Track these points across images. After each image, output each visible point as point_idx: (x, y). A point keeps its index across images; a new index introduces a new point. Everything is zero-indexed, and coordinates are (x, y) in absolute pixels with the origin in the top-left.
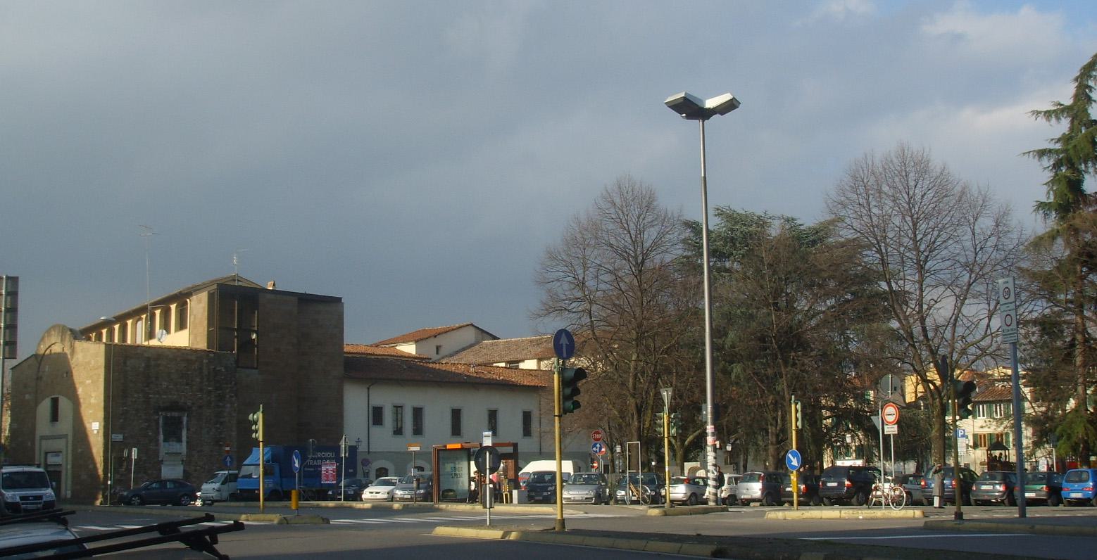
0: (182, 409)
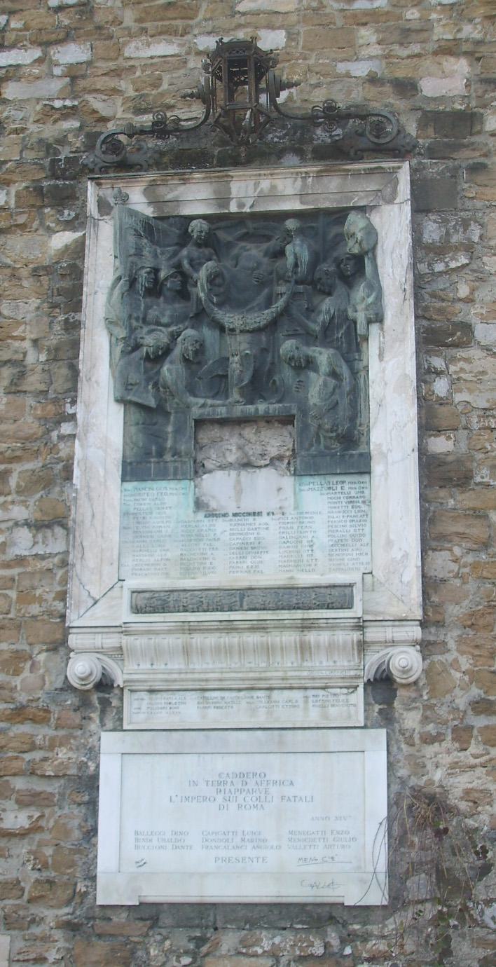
0: (350, 138)
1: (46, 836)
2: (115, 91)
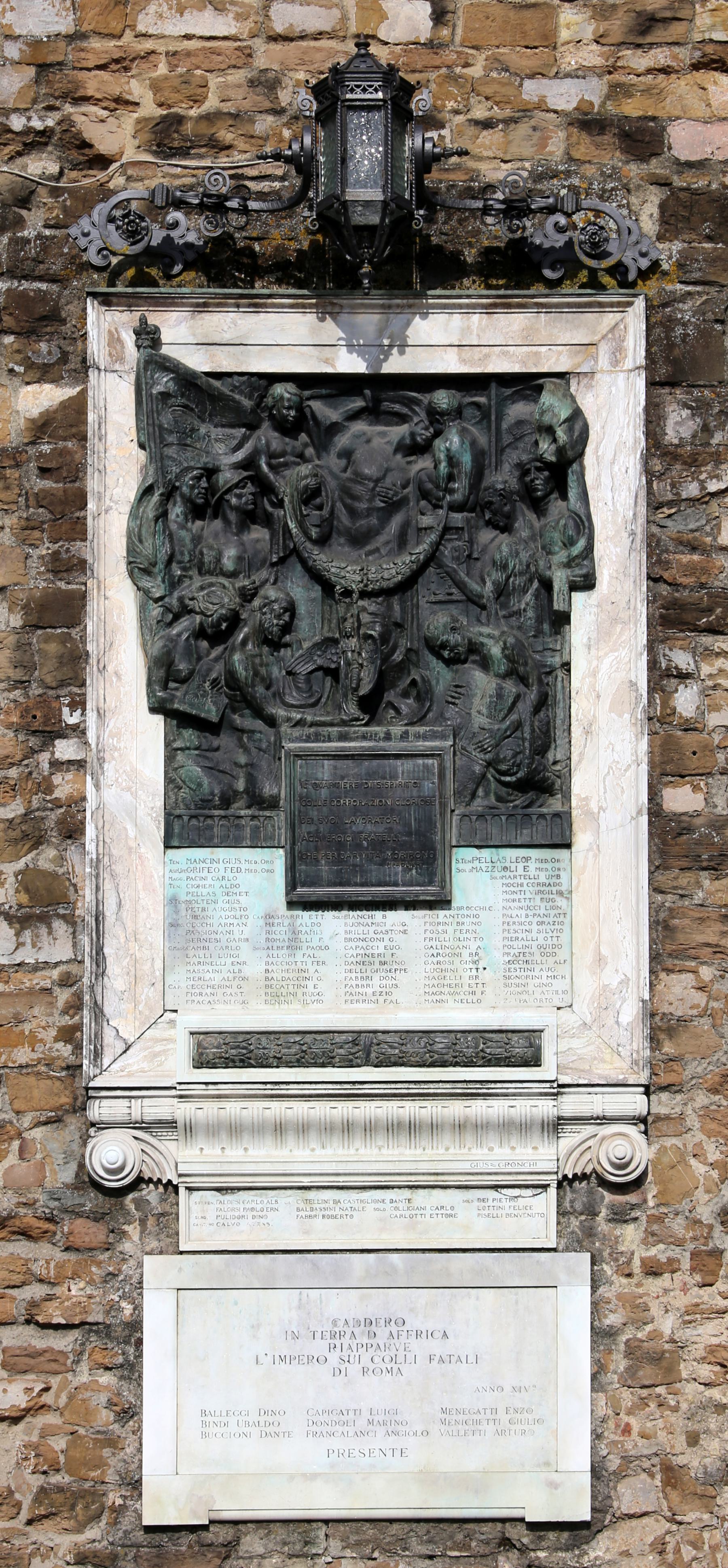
1: (51, 1419)
2: (121, 102)
